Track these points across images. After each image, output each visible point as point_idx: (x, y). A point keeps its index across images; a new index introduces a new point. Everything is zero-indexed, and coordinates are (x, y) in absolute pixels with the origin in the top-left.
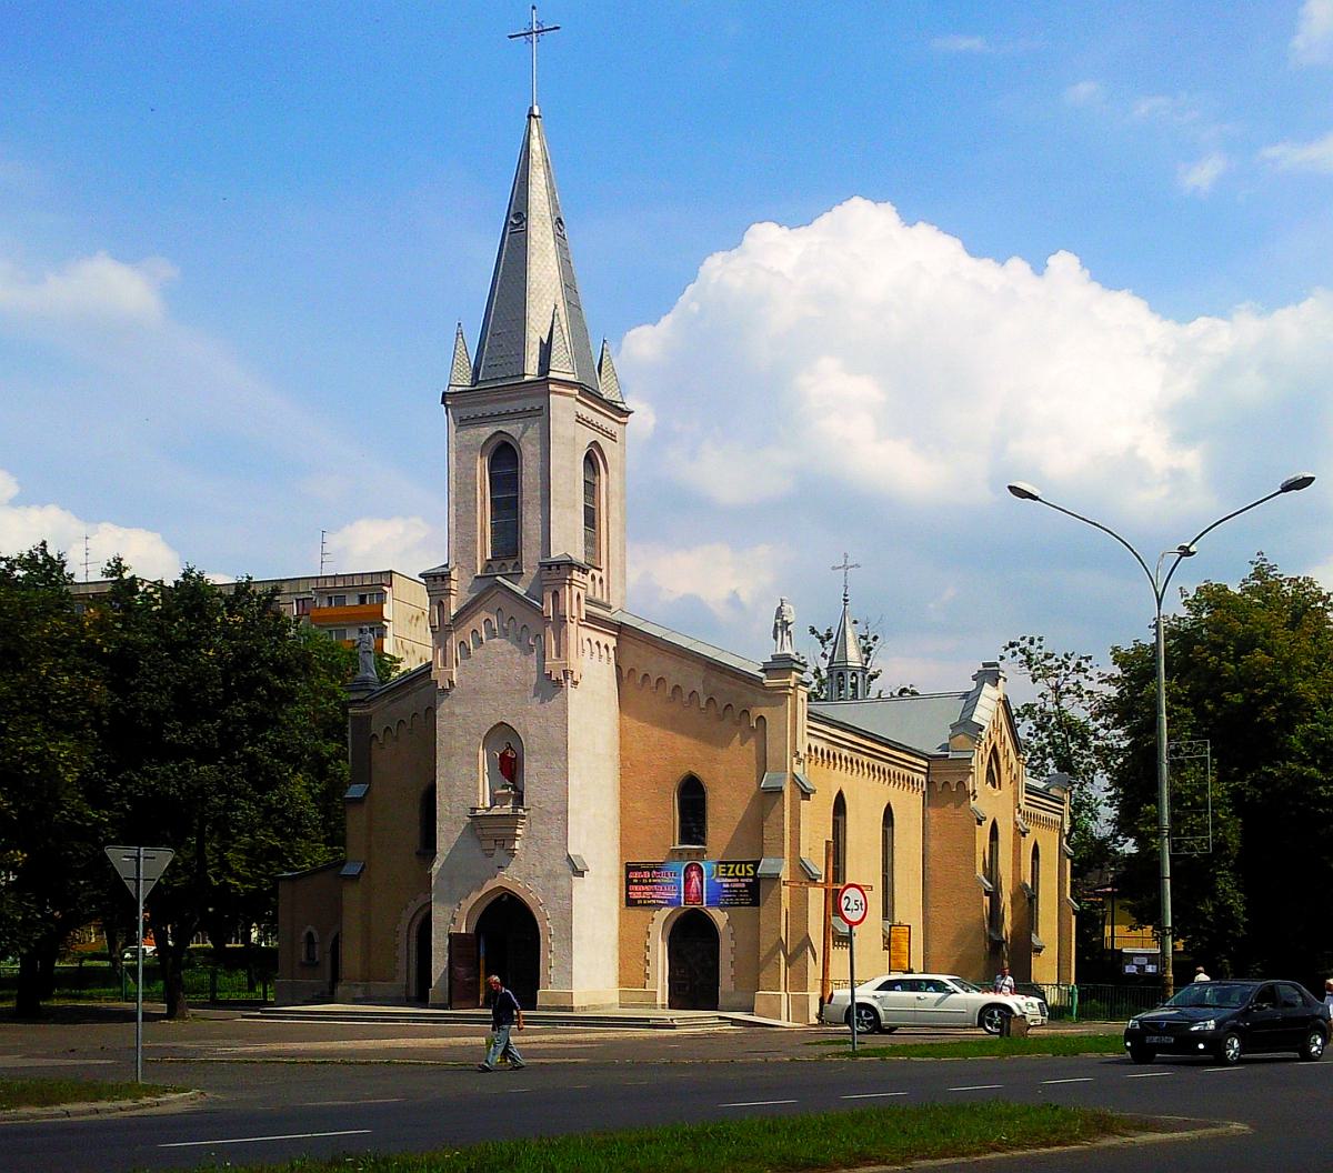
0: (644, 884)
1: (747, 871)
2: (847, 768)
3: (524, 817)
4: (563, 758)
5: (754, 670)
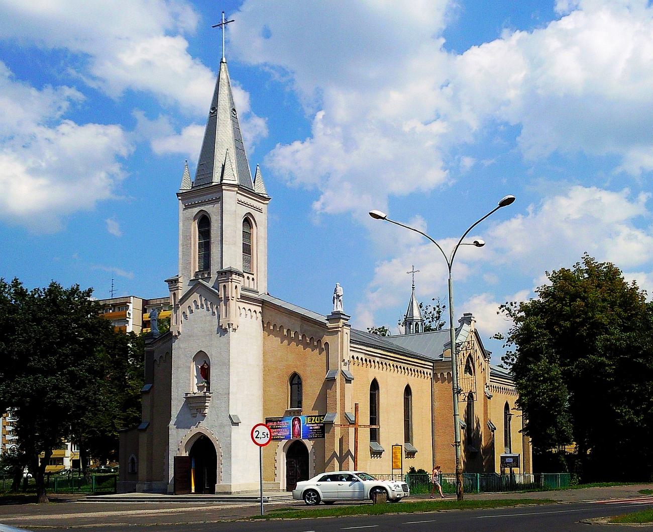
0: (274, 429)
1: (321, 420)
2: (379, 367)
3: (210, 397)
4: (228, 367)
5: (323, 319)
